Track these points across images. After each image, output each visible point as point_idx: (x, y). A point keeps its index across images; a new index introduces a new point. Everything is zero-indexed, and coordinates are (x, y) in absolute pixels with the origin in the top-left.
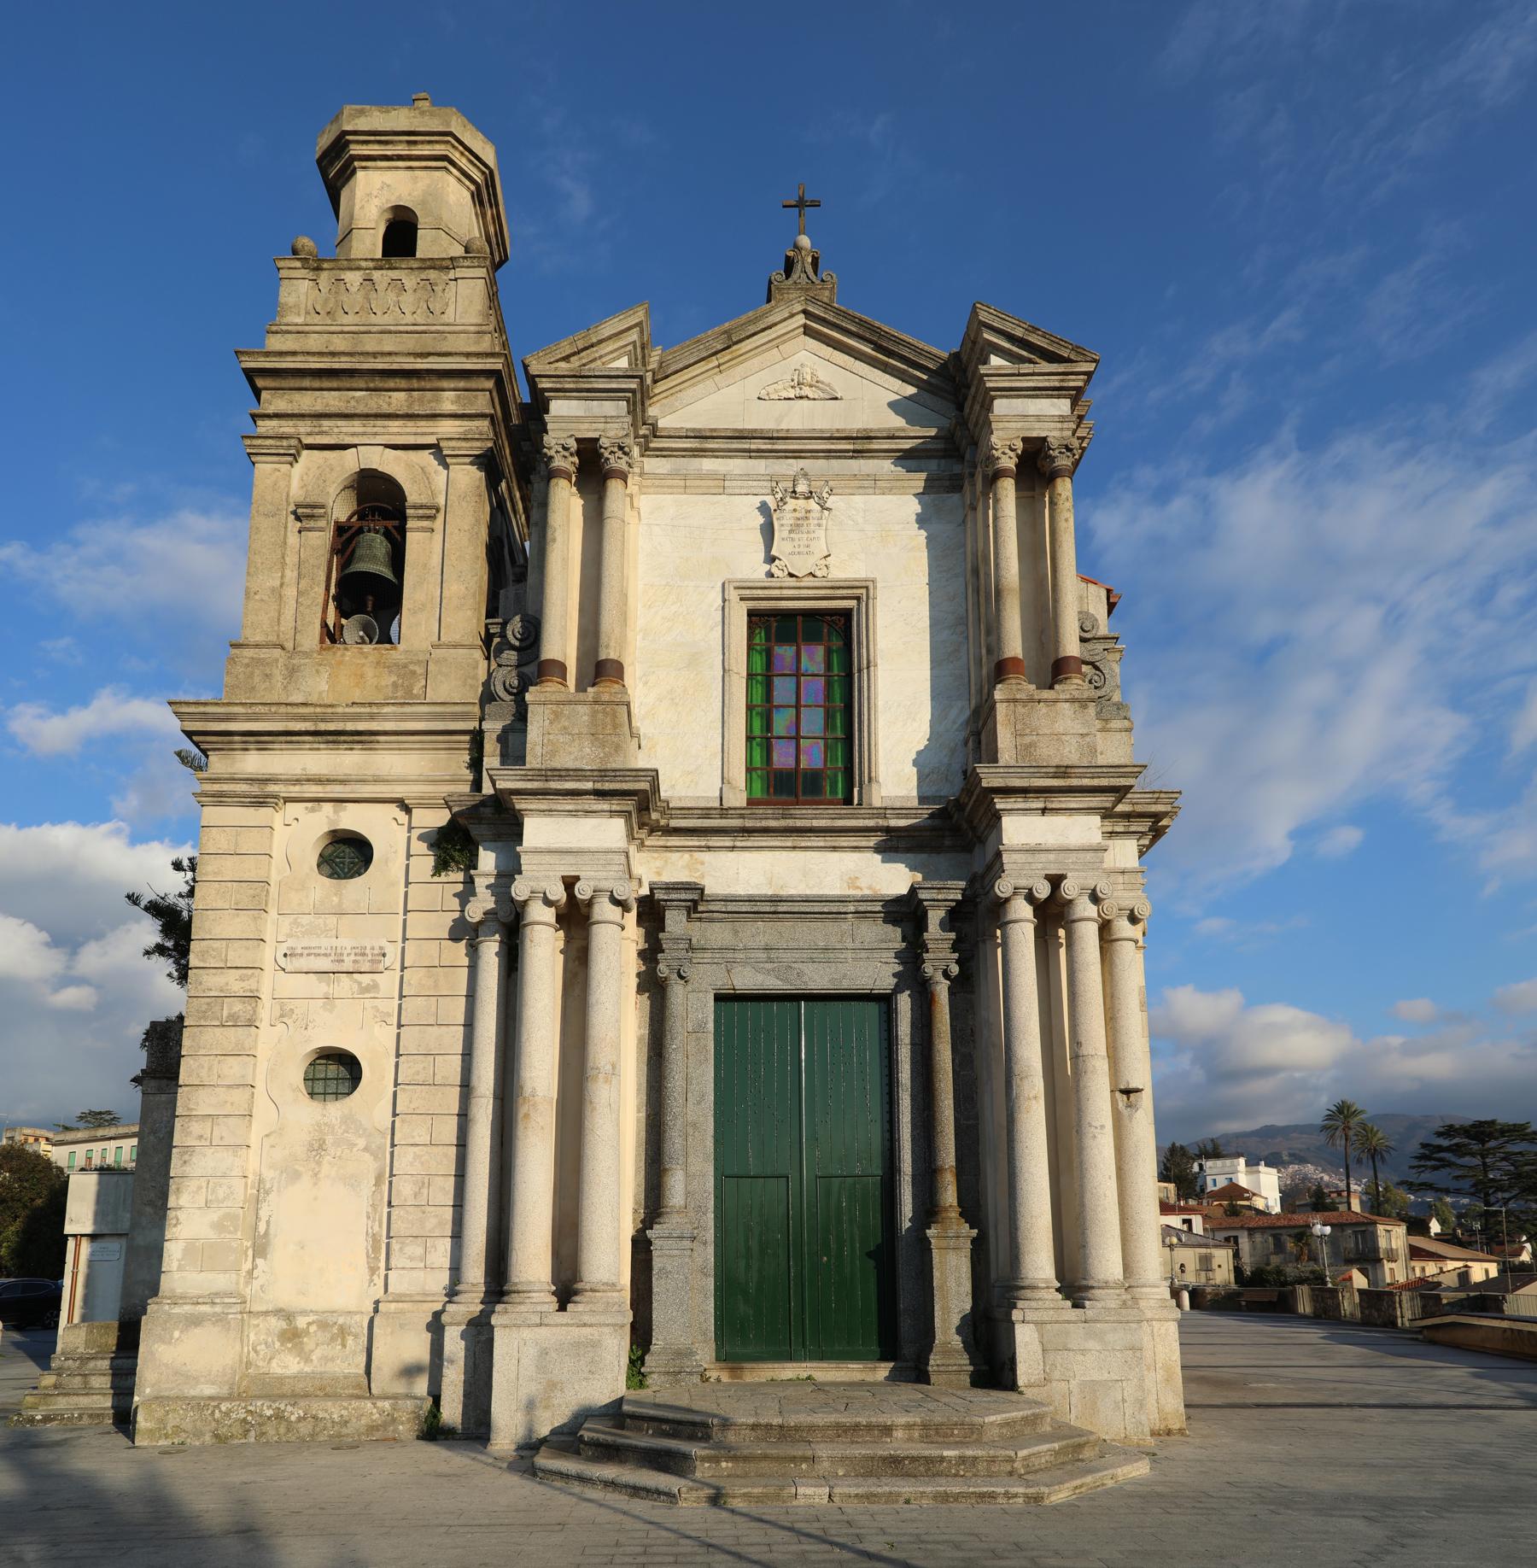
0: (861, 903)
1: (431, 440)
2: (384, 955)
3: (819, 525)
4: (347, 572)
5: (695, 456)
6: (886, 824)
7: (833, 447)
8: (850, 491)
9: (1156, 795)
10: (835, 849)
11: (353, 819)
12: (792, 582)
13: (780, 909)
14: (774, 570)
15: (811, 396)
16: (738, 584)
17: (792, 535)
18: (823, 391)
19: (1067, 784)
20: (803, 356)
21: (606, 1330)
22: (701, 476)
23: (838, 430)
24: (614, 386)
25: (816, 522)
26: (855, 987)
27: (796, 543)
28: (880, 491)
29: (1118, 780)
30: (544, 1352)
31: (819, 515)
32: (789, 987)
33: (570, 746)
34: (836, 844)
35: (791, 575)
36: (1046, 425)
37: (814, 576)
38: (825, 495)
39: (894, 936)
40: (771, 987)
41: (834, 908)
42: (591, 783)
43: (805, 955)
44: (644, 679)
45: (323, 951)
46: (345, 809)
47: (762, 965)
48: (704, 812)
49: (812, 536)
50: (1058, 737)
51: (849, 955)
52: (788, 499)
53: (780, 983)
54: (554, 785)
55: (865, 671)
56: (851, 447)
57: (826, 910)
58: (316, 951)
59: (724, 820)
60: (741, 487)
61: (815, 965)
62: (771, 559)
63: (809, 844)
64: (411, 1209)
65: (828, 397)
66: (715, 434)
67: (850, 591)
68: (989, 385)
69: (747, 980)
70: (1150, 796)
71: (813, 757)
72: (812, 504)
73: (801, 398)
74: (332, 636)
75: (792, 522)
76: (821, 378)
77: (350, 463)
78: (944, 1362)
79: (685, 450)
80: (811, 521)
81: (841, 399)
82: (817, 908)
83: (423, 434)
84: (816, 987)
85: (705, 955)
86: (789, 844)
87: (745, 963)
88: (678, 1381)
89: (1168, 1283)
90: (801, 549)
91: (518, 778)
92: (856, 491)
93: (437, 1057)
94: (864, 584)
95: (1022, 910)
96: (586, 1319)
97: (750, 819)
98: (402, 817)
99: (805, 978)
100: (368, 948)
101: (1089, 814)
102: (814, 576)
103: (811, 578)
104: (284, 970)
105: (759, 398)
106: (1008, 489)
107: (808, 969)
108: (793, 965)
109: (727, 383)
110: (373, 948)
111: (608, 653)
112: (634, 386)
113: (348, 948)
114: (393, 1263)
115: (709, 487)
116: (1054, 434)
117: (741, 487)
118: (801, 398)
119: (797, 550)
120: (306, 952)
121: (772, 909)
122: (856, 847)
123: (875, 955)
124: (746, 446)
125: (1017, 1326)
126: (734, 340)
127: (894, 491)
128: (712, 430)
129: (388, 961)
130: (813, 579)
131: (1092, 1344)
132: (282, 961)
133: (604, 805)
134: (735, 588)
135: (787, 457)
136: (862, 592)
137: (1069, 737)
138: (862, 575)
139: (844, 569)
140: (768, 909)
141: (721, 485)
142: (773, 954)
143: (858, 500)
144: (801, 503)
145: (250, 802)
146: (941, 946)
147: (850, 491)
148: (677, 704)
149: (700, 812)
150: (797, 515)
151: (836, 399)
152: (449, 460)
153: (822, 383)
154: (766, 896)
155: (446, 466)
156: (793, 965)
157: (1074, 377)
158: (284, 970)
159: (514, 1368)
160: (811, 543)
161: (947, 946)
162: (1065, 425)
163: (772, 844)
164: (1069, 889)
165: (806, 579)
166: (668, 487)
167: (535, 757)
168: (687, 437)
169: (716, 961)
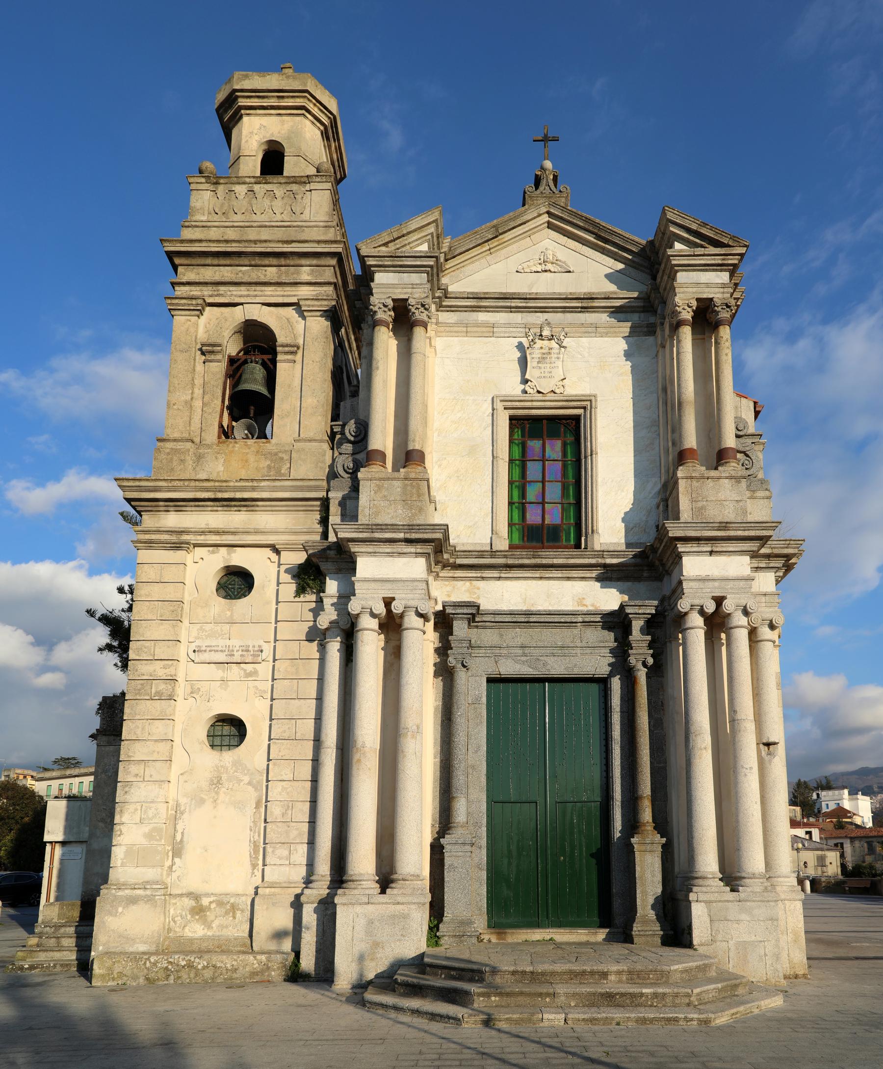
1: (294, 300)
2: (262, 651)
3: (558, 358)
4: (236, 390)
5: (474, 311)
7: (567, 305)
8: (579, 335)
9: (788, 542)
10: (568, 578)
11: (240, 558)
12: (540, 397)
13: (531, 620)
14: (527, 389)
15: (552, 270)
16: (502, 398)
17: (539, 365)
18: (561, 266)
20: (547, 243)
21: (413, 907)
22: (477, 325)
24: (418, 263)
25: (556, 356)
29: (761, 532)
31: (557, 351)
33: (388, 509)
35: (539, 392)
37: (555, 393)
38: (562, 338)
39: (609, 638)
41: (568, 619)
45: (220, 648)
46: (235, 552)
47: (519, 658)
48: (480, 553)
49: (553, 365)
51: (578, 651)
52: (537, 340)
53: (531, 670)
54: (377, 535)
55: (589, 457)
56: (580, 305)
58: (216, 648)
60: (505, 332)
61: (556, 658)
62: (525, 381)
64: (280, 824)
66: (487, 296)
67: (579, 403)
68: (674, 262)
69: (509, 668)
70: (784, 542)
71: (554, 516)
72: (553, 344)
73: (546, 271)
74: (226, 433)
75: (540, 356)
76: (559, 258)
77: (238, 315)
80: (552, 355)
82: (556, 619)
83: (288, 296)
85: (481, 651)
87: (507, 656)
88: (462, 942)
90: (546, 374)
91: (353, 530)
93: (297, 721)
94: (588, 398)
95: (696, 621)
96: (400, 899)
97: (510, 558)
98: (274, 557)
99: (548, 667)
100: (251, 646)
101: (742, 555)
102: (555, 393)
103: (553, 394)
104: (193, 661)
105: (517, 272)
106: (686, 333)
107: (551, 660)
110: (254, 647)
111: (414, 445)
112: (432, 263)
113: (237, 647)
114: (268, 861)
115: (483, 332)
116: (718, 296)
117: (505, 332)
118: (546, 271)
119: (543, 375)
120: (208, 649)
121: (526, 620)
123: (596, 651)
124: (509, 304)
125: (693, 904)
127: (609, 335)
128: (485, 293)
129: (264, 655)
130: (541, 395)
132: (192, 655)
133: (411, 549)
134: (501, 401)
135: (536, 312)
136: (587, 404)
138: (588, 392)
139: (575, 388)
140: (523, 620)
141: (491, 330)
145: (171, 547)
149: (477, 553)
150: (543, 351)
152: (306, 314)
153: (560, 261)
155: (304, 318)
156: (540, 658)
158: (193, 661)
161: (645, 645)
162: (726, 290)
164: (729, 606)
165: (549, 395)
166: (456, 332)
167: (365, 516)
168: (468, 298)
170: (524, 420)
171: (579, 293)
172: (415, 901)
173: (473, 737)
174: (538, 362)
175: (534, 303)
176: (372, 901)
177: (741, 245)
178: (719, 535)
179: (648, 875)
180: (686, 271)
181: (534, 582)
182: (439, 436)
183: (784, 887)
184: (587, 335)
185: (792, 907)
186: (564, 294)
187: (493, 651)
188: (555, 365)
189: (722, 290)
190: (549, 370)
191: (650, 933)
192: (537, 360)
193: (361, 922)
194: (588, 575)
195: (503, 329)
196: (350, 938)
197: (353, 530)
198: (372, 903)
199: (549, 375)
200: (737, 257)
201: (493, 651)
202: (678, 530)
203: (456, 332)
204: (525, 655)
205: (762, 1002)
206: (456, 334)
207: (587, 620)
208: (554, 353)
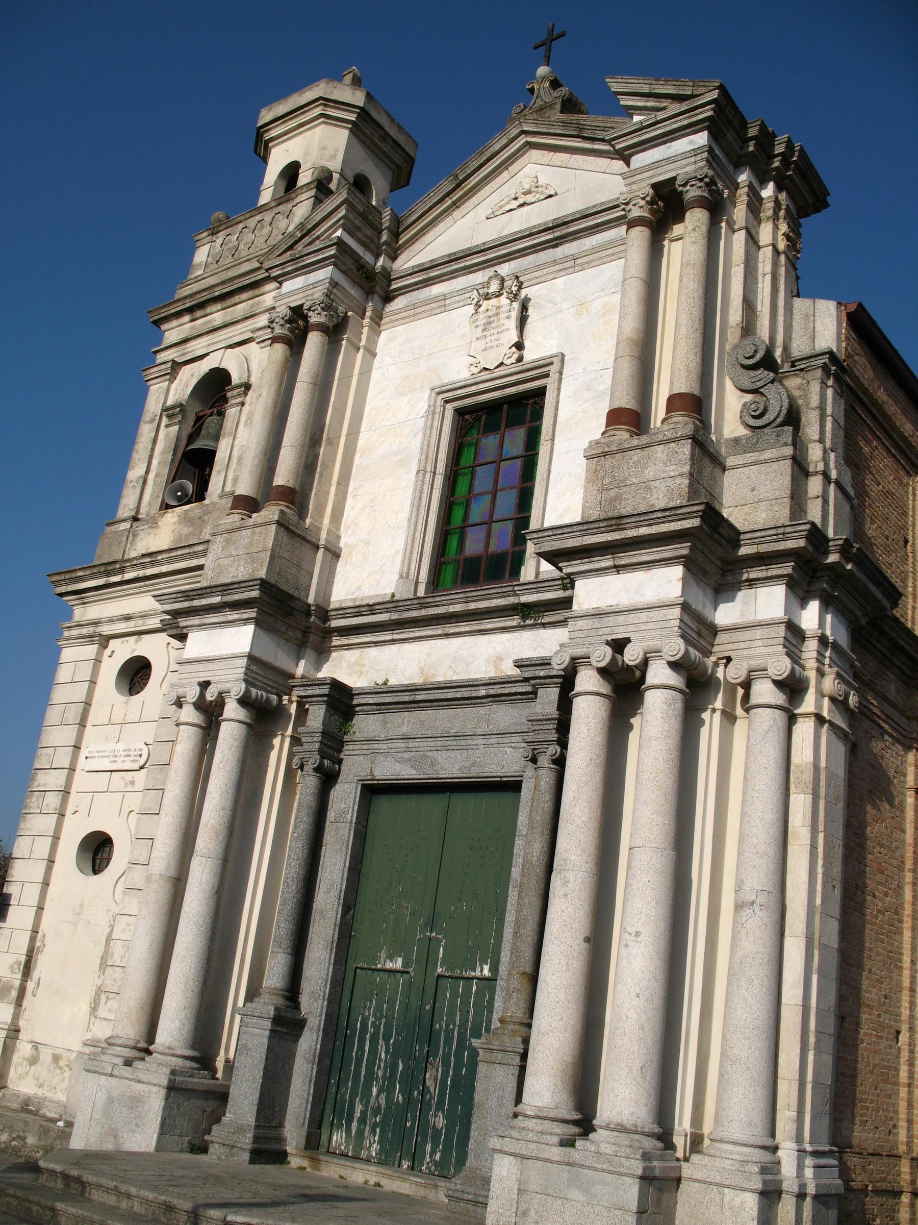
0: (492, 687)
4: (192, 447)
5: (427, 286)
6: (516, 601)
8: (552, 276)
9: (781, 531)
10: (447, 635)
13: (419, 698)
16: (438, 390)
17: (484, 334)
19: (622, 537)
22: (426, 302)
23: (534, 226)
25: (505, 315)
26: (483, 775)
27: (488, 340)
28: (580, 268)
29: (679, 523)
30: (111, 1100)
31: (507, 308)
32: (423, 776)
34: (482, 627)
36: (678, 164)
40: (406, 777)
41: (466, 693)
42: (220, 597)
43: (439, 744)
44: (354, 494)
48: (356, 610)
50: (646, 485)
51: (480, 741)
53: (414, 772)
54: (196, 603)
57: (458, 696)
59: (374, 616)
60: (459, 301)
61: (448, 753)
63: (457, 630)
65: (542, 197)
66: (434, 264)
67: (538, 371)
70: (773, 532)
75: (484, 321)
78: (464, 1188)
79: (416, 284)
81: (556, 194)
84: (447, 776)
85: (356, 747)
86: (439, 632)
87: (386, 754)
88: (232, 1155)
89: (579, 1143)
91: (173, 600)
92: (558, 275)
99: (437, 767)
101: (667, 565)
103: (484, 373)
105: (488, 218)
108: (428, 754)
109: (462, 215)
112: (333, 252)
115: (434, 309)
117: (459, 301)
119: (489, 345)
121: (411, 698)
122: (480, 631)
123: (506, 740)
124: (462, 265)
126: (461, 178)
130: (488, 372)
131: (574, 1194)
133: (233, 615)
137: (657, 482)
141: (443, 304)
142: (411, 744)
143: (560, 282)
144: (493, 301)
145: (89, 641)
146: (546, 727)
147: (552, 276)
148: (375, 511)
149: (352, 610)
150: (489, 313)
151: (550, 196)
154: (402, 686)
156: (428, 754)
157: (700, 110)
159: (90, 1110)
160: (501, 335)
161: (552, 726)
162: (699, 157)
163: (418, 634)
166: (402, 319)
169: (364, 752)
170: (479, 410)
171: (546, 223)
172: (155, 1081)
173: (328, 870)
174: (483, 330)
175: (493, 253)
176: (116, 1072)
177: (711, 88)
178: (610, 539)
179: (493, 1102)
180: (643, 151)
181: (439, 641)
182: (360, 457)
183: (726, 1162)
184: (562, 273)
185: (737, 1200)
186: (526, 230)
187: (371, 747)
188: (504, 328)
189: (693, 159)
190: (496, 336)
191: (470, 1197)
192: (482, 328)
193: (102, 1097)
194: (508, 624)
195: (457, 298)
196: (88, 1116)
197: (173, 600)
198: (116, 1077)
199: (496, 343)
200: (709, 107)
201: (371, 747)
202: (548, 541)
203: (402, 319)
204: (408, 750)
205: (125, 1186)
206: (402, 322)
207: (492, 692)
208: (503, 313)
